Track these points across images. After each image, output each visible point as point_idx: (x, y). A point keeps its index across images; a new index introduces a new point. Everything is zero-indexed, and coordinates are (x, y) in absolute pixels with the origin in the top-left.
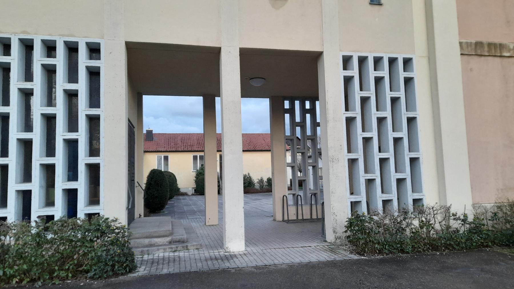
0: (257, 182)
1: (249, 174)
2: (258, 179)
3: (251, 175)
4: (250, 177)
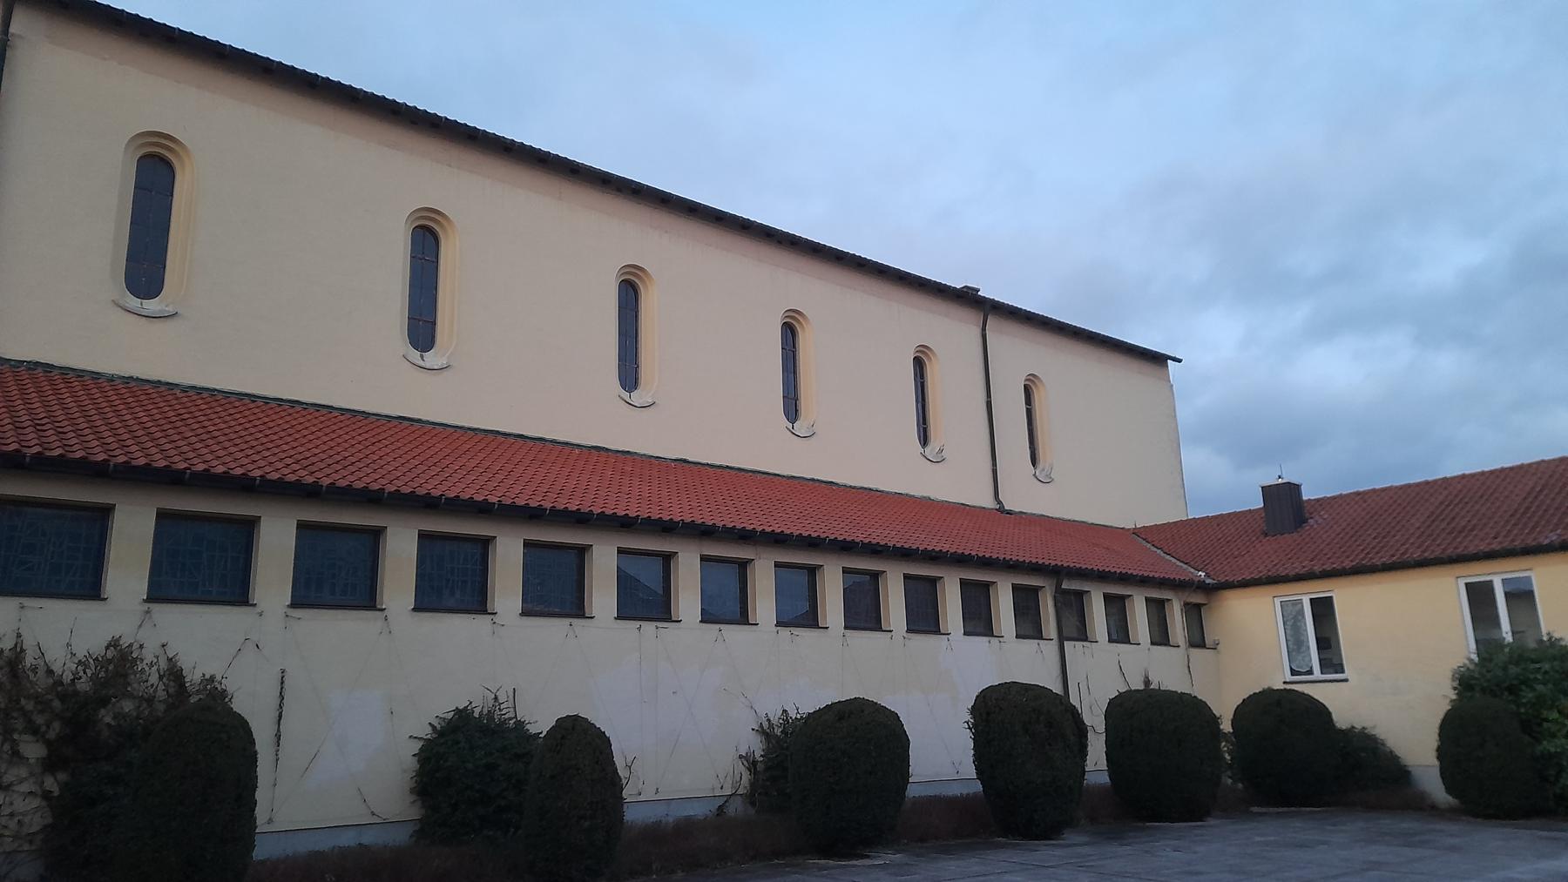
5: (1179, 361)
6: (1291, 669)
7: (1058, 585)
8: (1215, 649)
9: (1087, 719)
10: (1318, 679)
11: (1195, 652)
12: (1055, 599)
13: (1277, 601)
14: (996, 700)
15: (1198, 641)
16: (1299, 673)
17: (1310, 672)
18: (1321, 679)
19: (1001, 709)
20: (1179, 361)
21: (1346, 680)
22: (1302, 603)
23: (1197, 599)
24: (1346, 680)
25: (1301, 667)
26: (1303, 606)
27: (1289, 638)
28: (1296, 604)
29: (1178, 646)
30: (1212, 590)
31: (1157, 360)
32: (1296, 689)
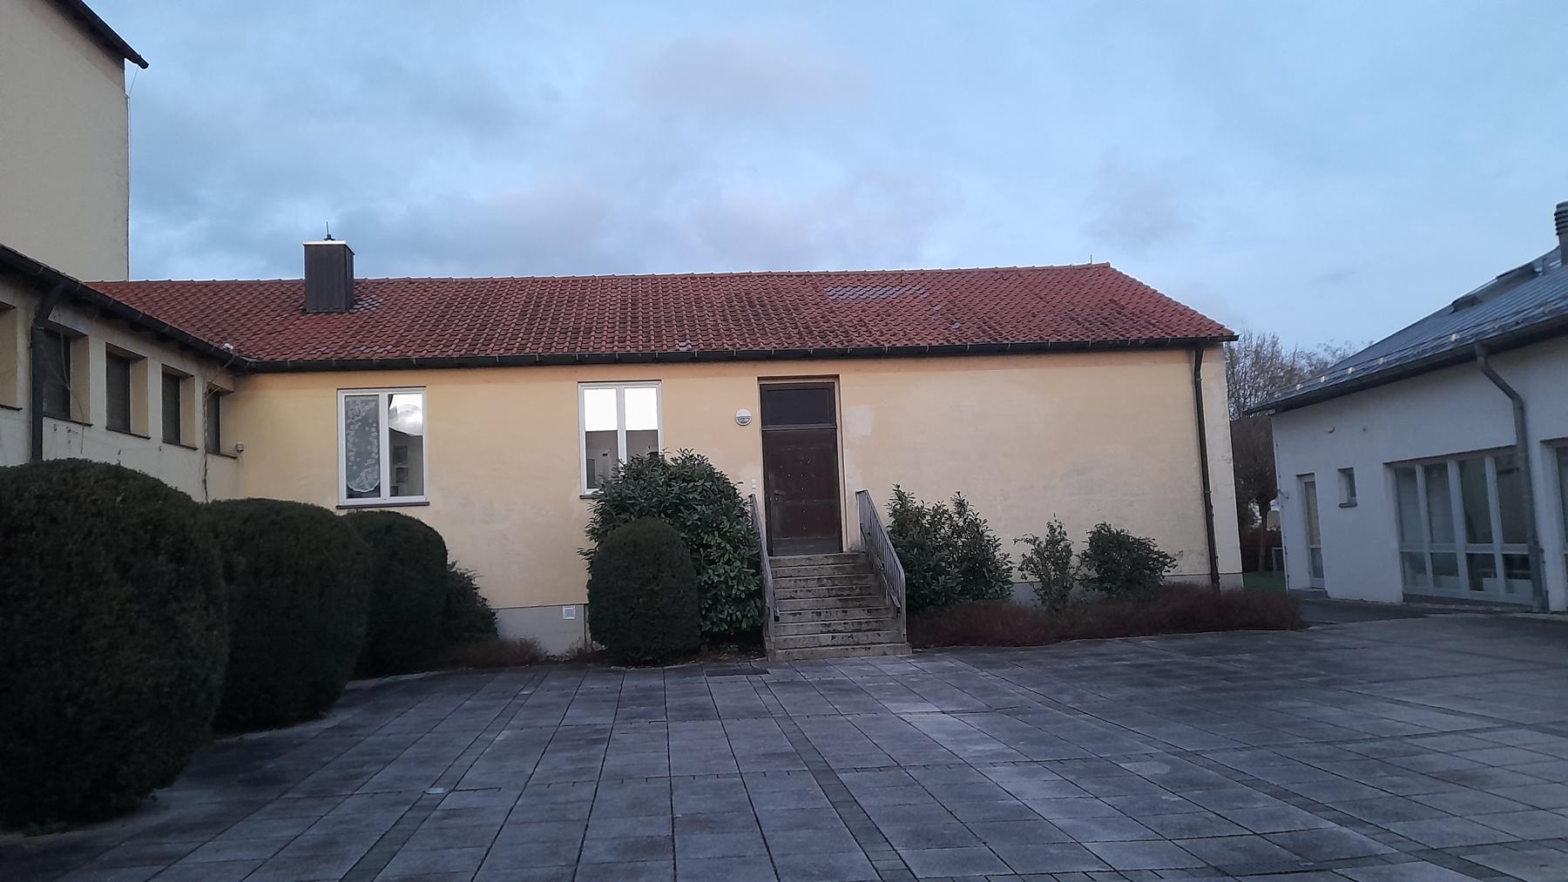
0: (1028, 561)
1: (961, 505)
2: (1034, 541)
3: (976, 508)
4: (974, 528)
5: (144, 65)
6: (347, 486)
7: (41, 316)
8: (235, 458)
9: (744, 492)
10: (386, 502)
11: (215, 462)
12: (33, 346)
13: (342, 395)
14: (40, 497)
15: (215, 446)
16: (360, 495)
17: (377, 491)
18: (346, 504)
19: (54, 520)
20: (144, 65)
21: (427, 504)
22: (377, 402)
23: (223, 383)
24: (427, 504)
25: (362, 488)
26: (377, 406)
27: (350, 447)
28: (367, 402)
29: (195, 449)
30: (243, 370)
31: (115, 50)
32: (409, 515)
